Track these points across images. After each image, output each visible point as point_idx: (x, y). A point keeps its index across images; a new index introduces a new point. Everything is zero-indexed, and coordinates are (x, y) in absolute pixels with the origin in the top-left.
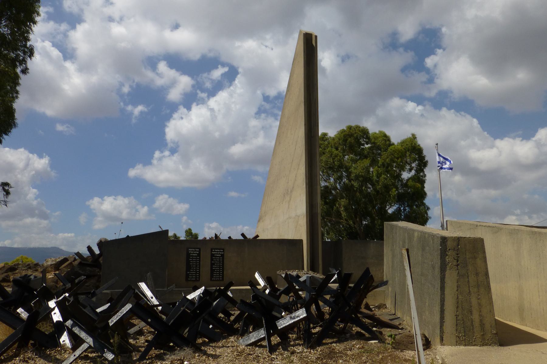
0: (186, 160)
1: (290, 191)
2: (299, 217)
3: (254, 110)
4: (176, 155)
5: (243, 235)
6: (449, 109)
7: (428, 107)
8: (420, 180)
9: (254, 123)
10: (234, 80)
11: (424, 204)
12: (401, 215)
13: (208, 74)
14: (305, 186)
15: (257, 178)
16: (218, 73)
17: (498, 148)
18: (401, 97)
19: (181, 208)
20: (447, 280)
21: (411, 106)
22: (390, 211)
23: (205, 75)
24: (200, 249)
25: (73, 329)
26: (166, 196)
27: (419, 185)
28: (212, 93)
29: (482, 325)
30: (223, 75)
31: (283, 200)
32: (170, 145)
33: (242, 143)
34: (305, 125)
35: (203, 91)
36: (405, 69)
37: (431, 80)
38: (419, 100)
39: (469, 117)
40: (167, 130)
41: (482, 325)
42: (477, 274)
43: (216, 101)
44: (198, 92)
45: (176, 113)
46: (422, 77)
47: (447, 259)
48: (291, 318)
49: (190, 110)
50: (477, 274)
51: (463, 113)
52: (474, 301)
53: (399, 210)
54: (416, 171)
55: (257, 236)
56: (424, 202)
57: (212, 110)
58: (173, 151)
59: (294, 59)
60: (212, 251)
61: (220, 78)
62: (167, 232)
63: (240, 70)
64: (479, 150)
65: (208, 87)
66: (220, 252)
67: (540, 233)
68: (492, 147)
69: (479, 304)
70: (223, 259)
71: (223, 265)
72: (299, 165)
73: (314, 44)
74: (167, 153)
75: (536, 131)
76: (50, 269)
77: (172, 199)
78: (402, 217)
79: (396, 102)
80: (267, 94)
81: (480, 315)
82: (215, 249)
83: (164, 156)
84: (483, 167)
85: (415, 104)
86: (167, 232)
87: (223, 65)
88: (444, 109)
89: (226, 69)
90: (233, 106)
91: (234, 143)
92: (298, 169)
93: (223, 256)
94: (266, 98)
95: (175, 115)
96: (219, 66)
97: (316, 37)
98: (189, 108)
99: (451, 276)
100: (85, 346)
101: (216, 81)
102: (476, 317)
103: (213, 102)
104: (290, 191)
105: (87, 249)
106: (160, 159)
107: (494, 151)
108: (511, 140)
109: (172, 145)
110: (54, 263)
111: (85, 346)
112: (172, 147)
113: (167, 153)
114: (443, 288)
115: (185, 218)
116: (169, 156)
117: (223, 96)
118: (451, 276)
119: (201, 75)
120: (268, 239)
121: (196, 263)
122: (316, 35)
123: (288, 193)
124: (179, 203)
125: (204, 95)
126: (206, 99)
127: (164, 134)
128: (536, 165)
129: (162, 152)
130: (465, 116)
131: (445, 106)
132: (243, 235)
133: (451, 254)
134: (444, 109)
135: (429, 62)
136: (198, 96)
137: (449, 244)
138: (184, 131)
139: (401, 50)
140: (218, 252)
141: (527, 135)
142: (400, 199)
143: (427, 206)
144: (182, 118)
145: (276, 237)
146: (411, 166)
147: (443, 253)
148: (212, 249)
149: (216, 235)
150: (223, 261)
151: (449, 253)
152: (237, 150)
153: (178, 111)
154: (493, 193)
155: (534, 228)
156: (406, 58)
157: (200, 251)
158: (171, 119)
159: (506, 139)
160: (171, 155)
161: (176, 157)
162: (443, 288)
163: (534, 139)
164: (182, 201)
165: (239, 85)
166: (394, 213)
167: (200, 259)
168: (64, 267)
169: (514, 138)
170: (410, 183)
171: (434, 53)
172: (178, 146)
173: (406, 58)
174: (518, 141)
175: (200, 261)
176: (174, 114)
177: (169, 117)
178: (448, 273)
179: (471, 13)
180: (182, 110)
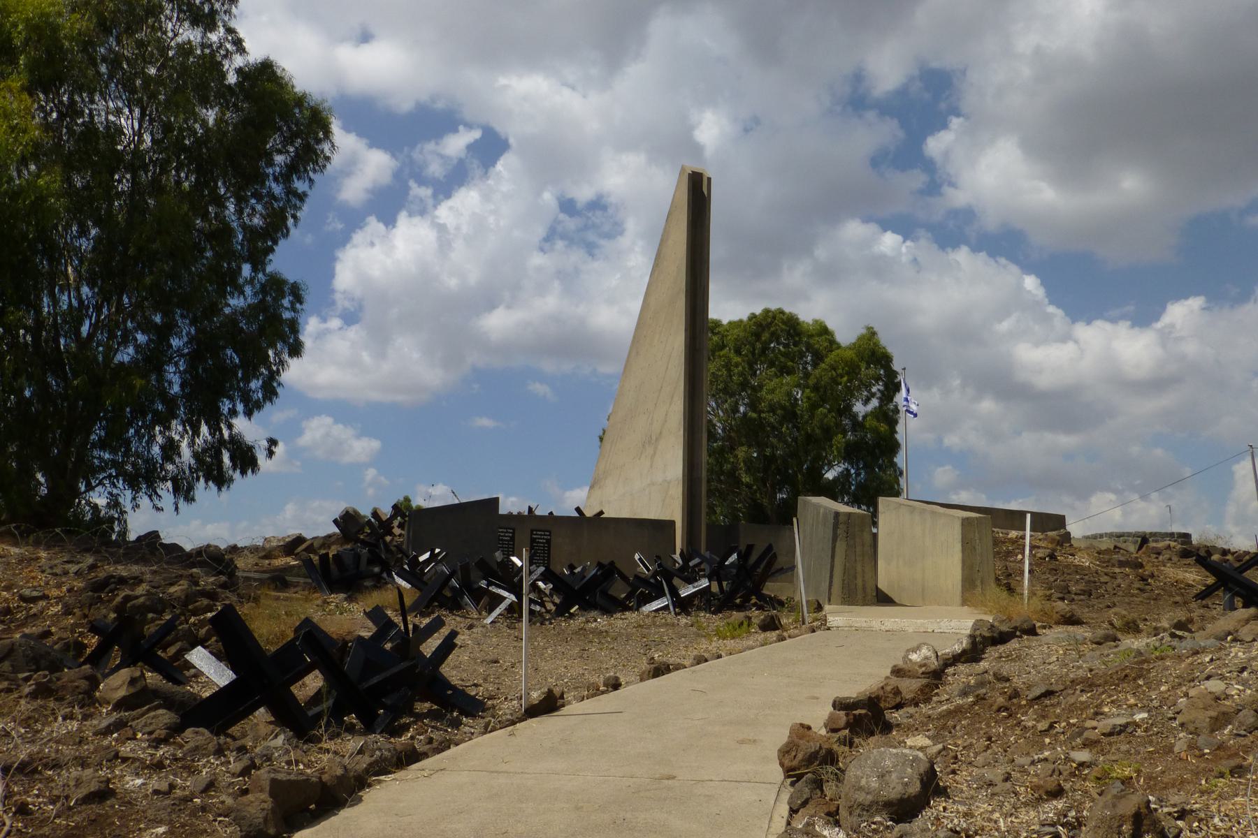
0: (380, 339)
1: (654, 438)
2: (669, 483)
3: (540, 231)
4: (355, 328)
5: (578, 510)
6: (975, 249)
7: (923, 242)
8: (888, 416)
9: (537, 260)
10: (493, 163)
11: (894, 465)
12: (851, 484)
13: (437, 144)
14: (682, 432)
15: (540, 389)
16: (457, 144)
17: (1076, 342)
18: (867, 220)
19: (362, 448)
20: (838, 550)
21: (889, 241)
22: (830, 475)
23: (430, 146)
24: (514, 530)
25: (490, 588)
26: (328, 420)
27: (883, 427)
28: (445, 188)
29: (864, 588)
30: (470, 147)
31: (641, 454)
32: (341, 303)
33: (509, 307)
34: (686, 330)
35: (422, 182)
36: (878, 161)
37: (934, 187)
38: (905, 227)
39: (1014, 269)
40: (339, 267)
41: (864, 588)
42: (863, 545)
43: (451, 208)
44: (412, 184)
45: (360, 232)
46: (917, 179)
47: (839, 531)
48: (694, 587)
49: (394, 227)
50: (863, 545)
51: (1003, 261)
52: (859, 569)
53: (846, 475)
54: (881, 399)
55: (602, 513)
56: (895, 460)
57: (441, 228)
58: (350, 318)
59: (670, 214)
60: (532, 534)
61: (463, 155)
62: (494, 502)
63: (512, 141)
64: (1037, 344)
65: (437, 175)
66: (545, 535)
67: (933, 512)
68: (1065, 338)
69: (863, 571)
70: (549, 547)
71: (549, 557)
72: (672, 398)
73: (706, 193)
74: (335, 323)
75: (1163, 309)
76: (276, 553)
77: (341, 426)
78: (853, 488)
79: (854, 230)
80: (569, 196)
81: (863, 581)
82: (537, 531)
83: (328, 332)
84: (1044, 382)
85: (899, 238)
86: (494, 502)
87: (469, 126)
88: (964, 249)
89: (476, 134)
90: (491, 219)
91: (491, 306)
92: (670, 404)
93: (548, 542)
94: (568, 206)
95: (358, 237)
96: (461, 128)
97: (709, 179)
98: (389, 221)
99: (841, 547)
100: (503, 606)
101: (455, 161)
102: (859, 582)
103: (444, 212)
104: (654, 438)
105: (515, 513)
106: (320, 336)
107: (1070, 347)
108: (1108, 326)
109: (347, 304)
110: (282, 543)
111: (503, 606)
112: (345, 309)
113: (335, 323)
114: (833, 557)
115: (371, 473)
116: (340, 329)
117: (467, 200)
118: (841, 547)
119: (419, 146)
120: (618, 518)
121: (508, 551)
122: (710, 176)
123: (652, 441)
124: (358, 437)
125: (425, 192)
126: (430, 202)
127: (331, 275)
128: (1156, 384)
129: (324, 320)
130: (1005, 267)
131: (967, 243)
132: (578, 510)
133: (842, 527)
134: (964, 249)
135: (935, 145)
136: (411, 193)
137: (841, 519)
138: (376, 272)
139: (871, 115)
140: (541, 535)
141: (1144, 318)
142: (850, 453)
143: (899, 468)
144: (372, 244)
145: (625, 514)
146: (869, 391)
147: (836, 526)
148: (532, 531)
149: (530, 509)
150: (549, 550)
151: (841, 526)
152: (498, 322)
153: (365, 229)
154: (1066, 441)
155: (959, 511)
156: (885, 132)
157: (513, 533)
158: (348, 246)
159: (1099, 323)
160: (345, 327)
161: (354, 333)
162: (833, 557)
163: (1159, 325)
164: (363, 433)
165: (505, 174)
166: (836, 480)
167: (513, 544)
168: (304, 550)
169: (1114, 321)
170: (870, 423)
171: (944, 126)
172: (361, 308)
173: (885, 132)
174: (1123, 328)
175: (513, 548)
176: (354, 232)
177: (344, 240)
178: (838, 544)
179: (1027, 41)
180: (374, 226)
